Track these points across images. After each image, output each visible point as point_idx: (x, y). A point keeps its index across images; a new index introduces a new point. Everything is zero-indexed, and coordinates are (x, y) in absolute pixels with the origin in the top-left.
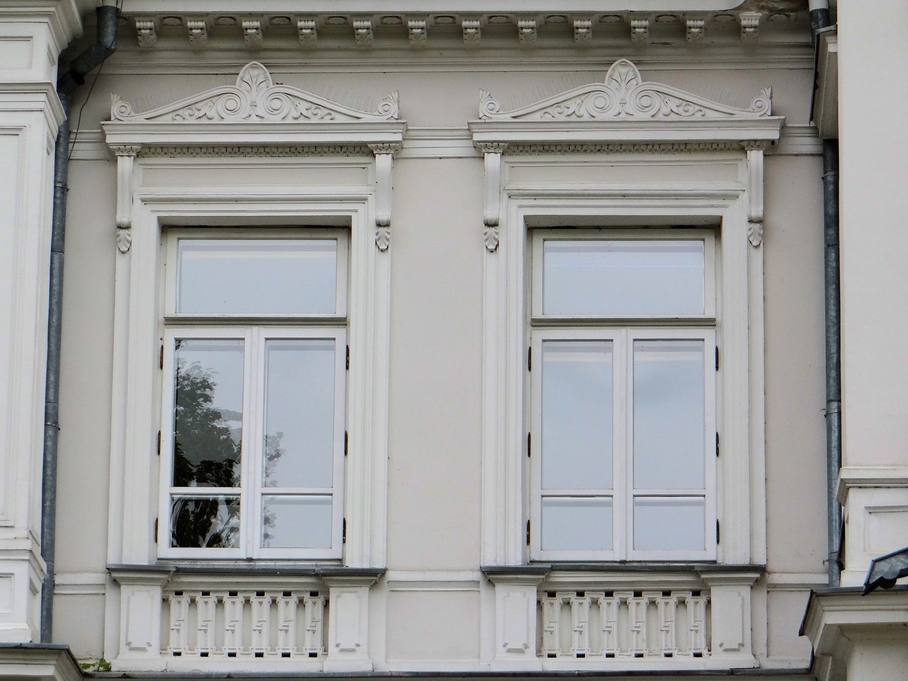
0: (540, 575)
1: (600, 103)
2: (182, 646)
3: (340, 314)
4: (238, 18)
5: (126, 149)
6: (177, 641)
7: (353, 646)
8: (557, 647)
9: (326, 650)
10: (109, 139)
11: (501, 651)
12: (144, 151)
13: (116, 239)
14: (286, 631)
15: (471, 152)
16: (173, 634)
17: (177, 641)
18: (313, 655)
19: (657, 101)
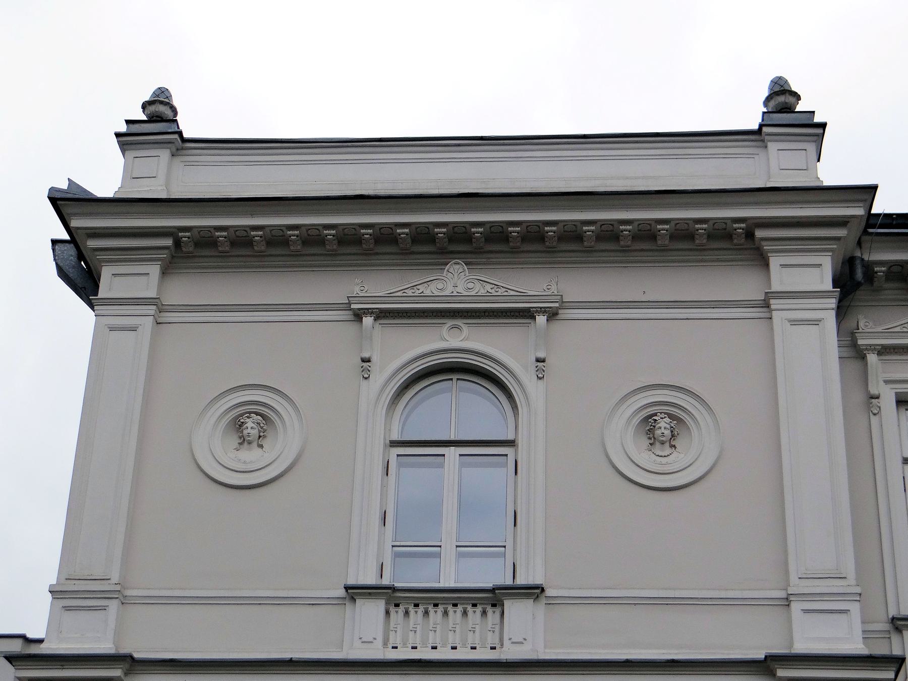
0: (392, 596)
1: (440, 286)
2: (457, 641)
3: (511, 437)
4: (394, 228)
5: (871, 348)
6: (394, 639)
7: (521, 640)
8: (457, 641)
9: (502, 645)
10: (860, 342)
11: (357, 643)
12: (884, 351)
13: (869, 406)
14: (435, 631)
15: (352, 317)
16: (392, 634)
17: (394, 639)
18: (493, 648)
19: (478, 285)
